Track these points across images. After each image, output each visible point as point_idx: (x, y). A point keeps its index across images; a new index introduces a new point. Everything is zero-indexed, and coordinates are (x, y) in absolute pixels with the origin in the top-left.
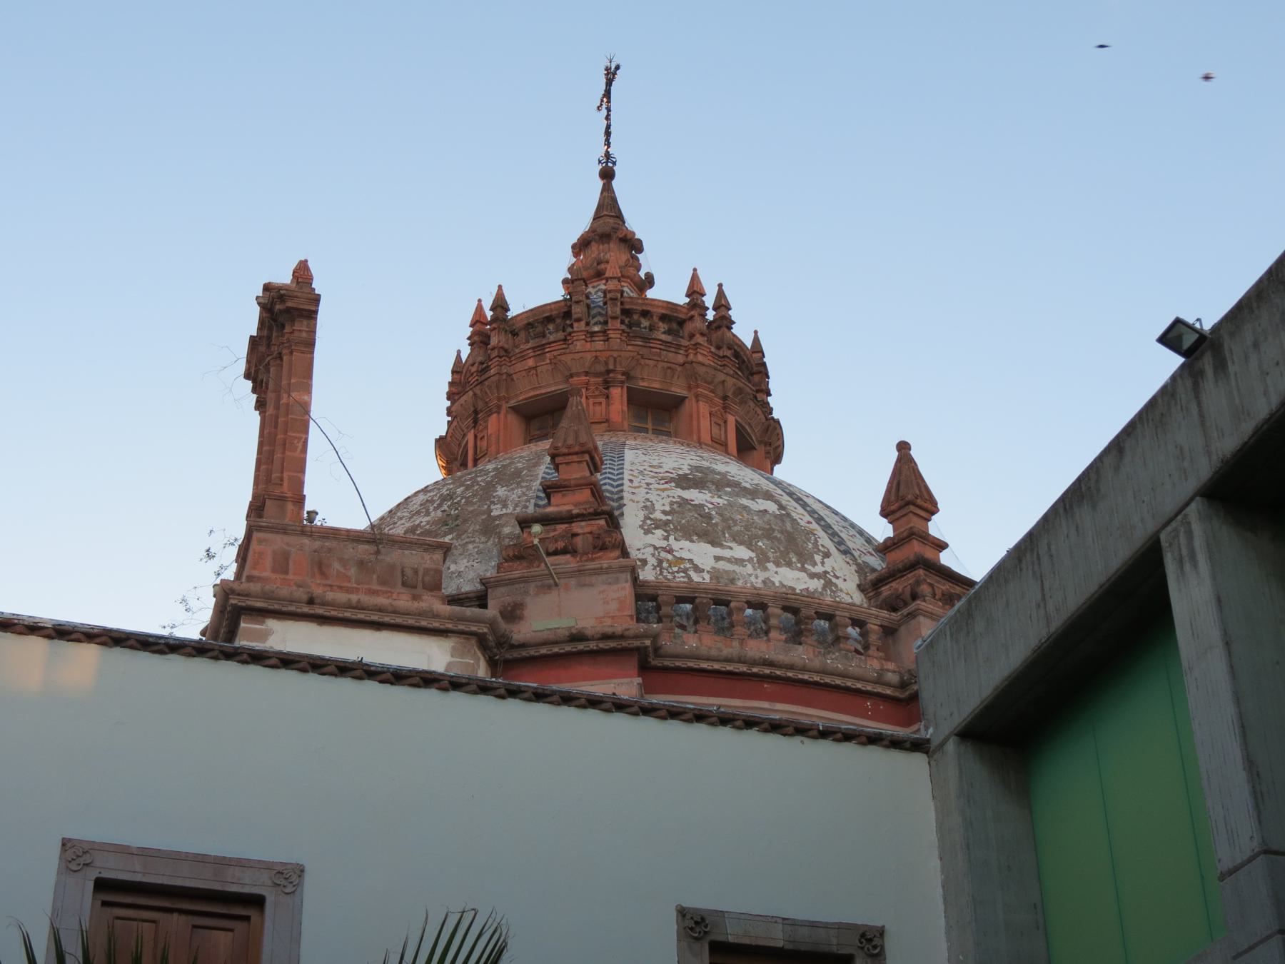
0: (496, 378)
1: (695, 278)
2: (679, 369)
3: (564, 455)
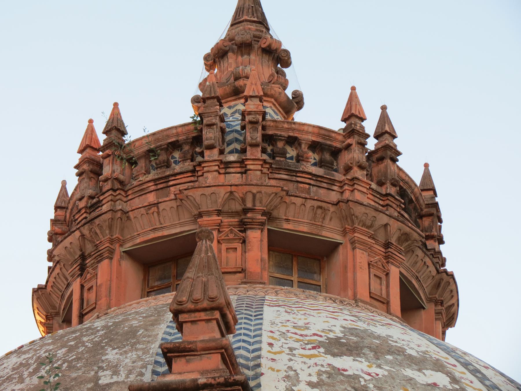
0: (109, 215)
1: (353, 98)
2: (332, 209)
3: (190, 311)
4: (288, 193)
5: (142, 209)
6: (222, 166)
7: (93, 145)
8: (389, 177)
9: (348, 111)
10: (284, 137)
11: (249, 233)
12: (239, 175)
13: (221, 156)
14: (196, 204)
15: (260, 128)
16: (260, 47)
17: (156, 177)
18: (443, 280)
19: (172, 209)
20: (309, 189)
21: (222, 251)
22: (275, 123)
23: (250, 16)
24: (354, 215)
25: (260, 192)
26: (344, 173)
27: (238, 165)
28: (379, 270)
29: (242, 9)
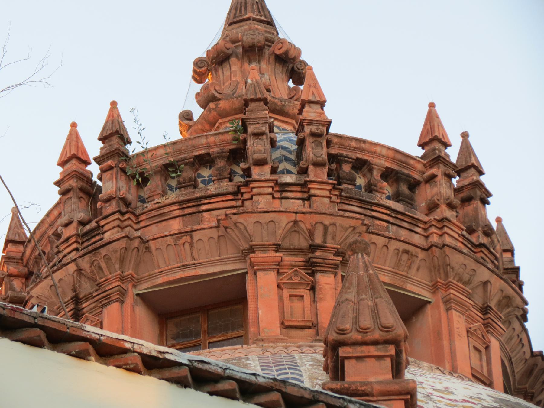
0: (123, 244)
1: (432, 118)
2: (422, 255)
3: (356, 344)
4: (368, 229)
5: (168, 238)
6: (277, 189)
7: (80, 155)
8: (480, 223)
9: (428, 133)
10: (351, 158)
11: (319, 277)
12: (300, 201)
13: (273, 175)
14: (247, 235)
15: (325, 144)
16: (274, 53)
17: (181, 199)
18: (537, 365)
19: (211, 239)
20: (387, 228)
21: (285, 299)
22: (339, 139)
23: (256, 13)
24: (449, 265)
25: (334, 224)
26: (426, 212)
27: (298, 189)
28: (479, 341)
29: (243, 4)
